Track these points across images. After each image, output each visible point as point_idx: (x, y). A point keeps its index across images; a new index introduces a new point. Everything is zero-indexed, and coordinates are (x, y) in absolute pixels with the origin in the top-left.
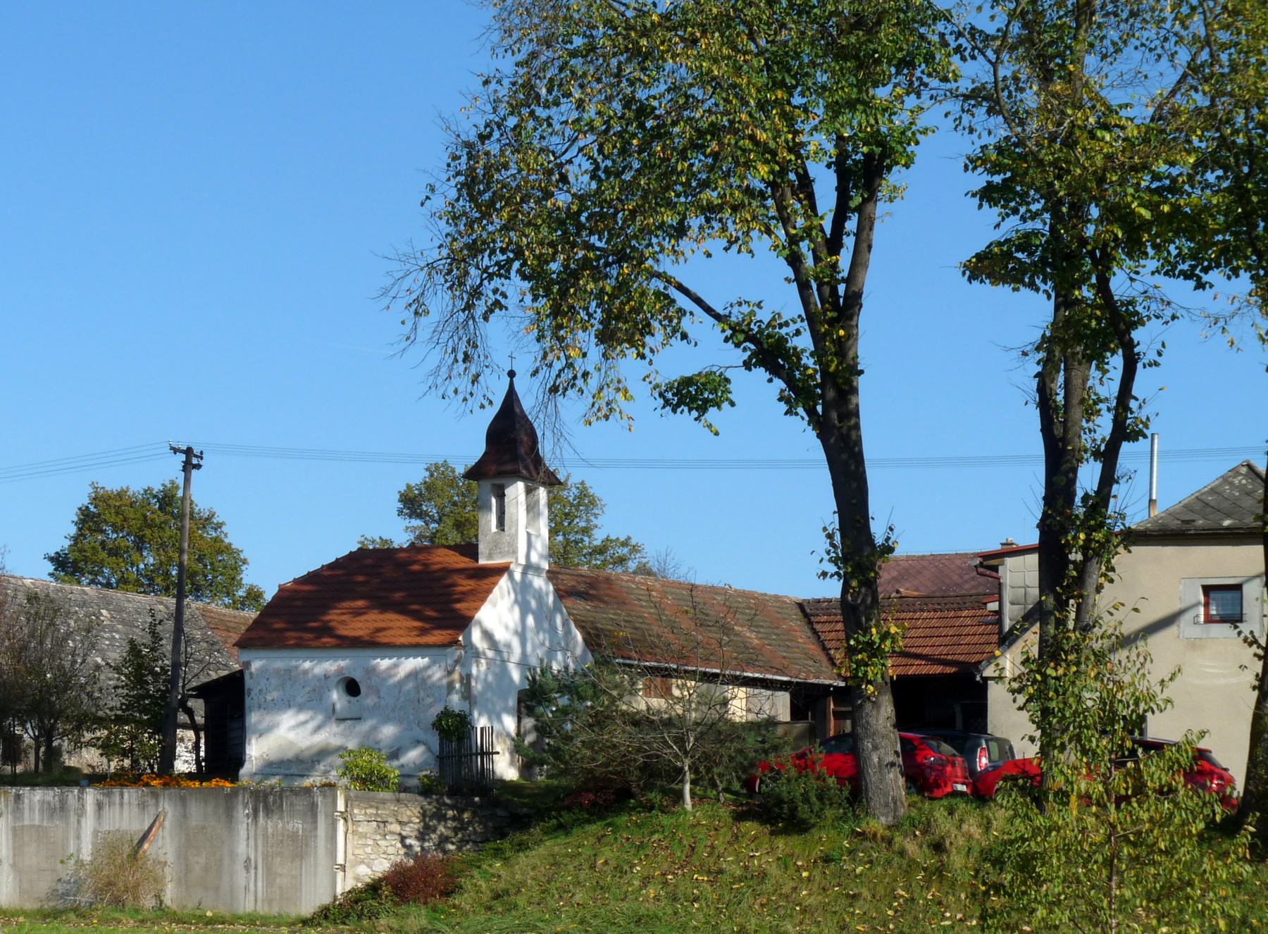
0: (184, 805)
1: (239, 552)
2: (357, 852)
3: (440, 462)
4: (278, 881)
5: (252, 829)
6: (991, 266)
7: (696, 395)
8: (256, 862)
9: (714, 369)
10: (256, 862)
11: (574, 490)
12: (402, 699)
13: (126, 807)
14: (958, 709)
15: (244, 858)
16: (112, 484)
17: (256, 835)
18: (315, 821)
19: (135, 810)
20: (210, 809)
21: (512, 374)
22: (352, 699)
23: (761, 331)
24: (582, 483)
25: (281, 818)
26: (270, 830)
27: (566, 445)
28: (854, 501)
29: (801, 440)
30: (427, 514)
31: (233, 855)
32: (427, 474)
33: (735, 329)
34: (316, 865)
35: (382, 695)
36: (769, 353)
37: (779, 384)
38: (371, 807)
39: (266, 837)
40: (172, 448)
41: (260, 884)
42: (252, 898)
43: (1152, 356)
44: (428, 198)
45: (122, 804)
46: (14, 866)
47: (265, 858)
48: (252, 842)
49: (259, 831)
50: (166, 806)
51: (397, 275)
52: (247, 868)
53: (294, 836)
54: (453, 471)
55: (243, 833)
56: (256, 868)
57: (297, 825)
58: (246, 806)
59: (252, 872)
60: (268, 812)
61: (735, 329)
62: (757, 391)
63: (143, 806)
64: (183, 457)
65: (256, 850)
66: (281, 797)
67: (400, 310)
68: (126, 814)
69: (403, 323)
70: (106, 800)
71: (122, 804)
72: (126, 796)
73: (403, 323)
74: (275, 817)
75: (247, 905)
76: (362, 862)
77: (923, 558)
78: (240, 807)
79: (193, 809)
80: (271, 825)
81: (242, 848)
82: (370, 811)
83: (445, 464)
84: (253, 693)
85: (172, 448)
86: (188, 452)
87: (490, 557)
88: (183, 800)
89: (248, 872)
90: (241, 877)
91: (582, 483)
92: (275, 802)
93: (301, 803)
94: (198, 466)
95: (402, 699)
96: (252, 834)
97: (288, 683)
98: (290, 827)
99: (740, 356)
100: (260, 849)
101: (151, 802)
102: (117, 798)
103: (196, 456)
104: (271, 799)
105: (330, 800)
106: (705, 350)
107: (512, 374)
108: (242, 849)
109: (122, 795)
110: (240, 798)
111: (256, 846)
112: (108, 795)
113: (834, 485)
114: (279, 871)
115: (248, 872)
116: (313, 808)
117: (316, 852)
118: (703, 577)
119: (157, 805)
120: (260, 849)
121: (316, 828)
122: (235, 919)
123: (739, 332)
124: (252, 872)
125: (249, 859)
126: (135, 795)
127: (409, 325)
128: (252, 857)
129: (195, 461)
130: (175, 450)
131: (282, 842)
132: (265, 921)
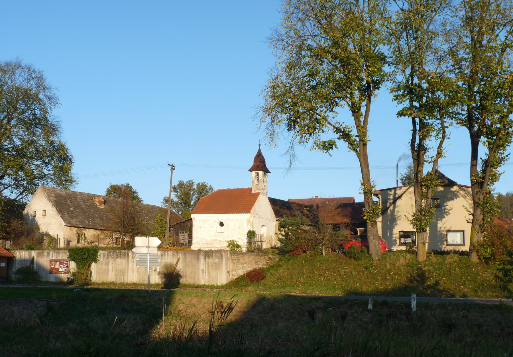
0: (185, 256)
6: (401, 114)
7: (328, 146)
14: (358, 230)
16: (115, 184)
19: (172, 256)
20: (193, 256)
21: (260, 145)
31: (199, 269)
36: (345, 136)
43: (448, 136)
46: (138, 272)
47: (208, 269)
53: (216, 264)
57: (217, 261)
58: (203, 255)
62: (342, 145)
63: (174, 255)
64: (171, 167)
67: (257, 121)
81: (201, 267)
88: (185, 254)
93: (218, 255)
99: (338, 136)
101: (176, 254)
102: (167, 253)
107: (260, 145)
112: (164, 253)
113: (228, 190)
116: (221, 256)
118: (324, 197)
123: (338, 130)
125: (203, 270)
130: (169, 165)
132: (208, 287)
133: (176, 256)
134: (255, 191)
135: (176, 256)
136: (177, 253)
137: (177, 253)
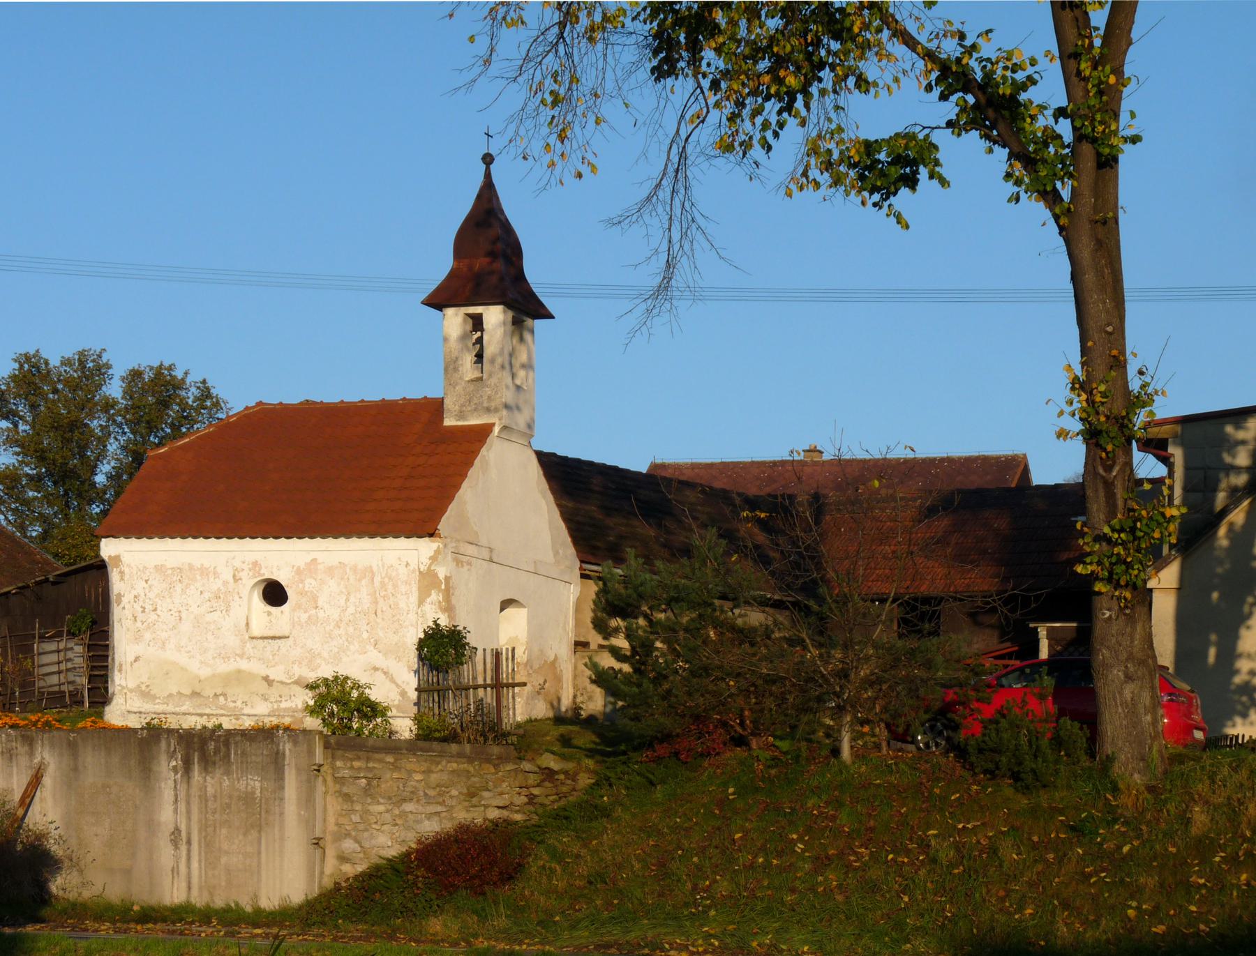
2: (342, 820)
3: (32, 352)
4: (224, 860)
5: (182, 789)
8: (189, 834)
10: (189, 834)
11: (193, 389)
12: (351, 610)
14: (1042, 633)
15: (171, 828)
17: (188, 796)
21: (488, 159)
22: (274, 609)
24: (204, 382)
25: (228, 773)
26: (210, 790)
27: (699, 236)
28: (1109, 329)
29: (1030, 241)
31: (152, 825)
32: (17, 366)
35: (320, 604)
36: (992, 107)
37: (1002, 153)
38: (359, 758)
39: (204, 798)
41: (195, 865)
42: (184, 885)
47: (203, 827)
48: (182, 807)
49: (194, 791)
50: (47, 755)
52: (175, 843)
54: (47, 363)
55: (167, 794)
56: (189, 842)
57: (254, 783)
58: (171, 756)
59: (184, 848)
60: (207, 763)
62: (974, 162)
65: (189, 819)
69: (472, 39)
73: (472, 39)
74: (218, 773)
75: (173, 894)
76: (348, 835)
77: (711, 466)
78: (163, 758)
79: (89, 759)
82: (356, 764)
84: (125, 600)
87: (461, 415)
88: (72, 747)
89: (176, 847)
90: (166, 854)
91: (204, 382)
92: (217, 751)
93: (259, 752)
95: (351, 610)
96: (182, 795)
97: (179, 587)
98: (242, 785)
100: (195, 816)
101: (22, 749)
104: (212, 746)
107: (488, 159)
108: (166, 815)
110: (163, 744)
111: (189, 812)
114: (225, 846)
115: (176, 847)
117: (282, 823)
119: (31, 754)
120: (195, 816)
121: (282, 788)
123: (951, 76)
125: (177, 830)
127: (483, 44)
128: (183, 827)
131: (229, 806)
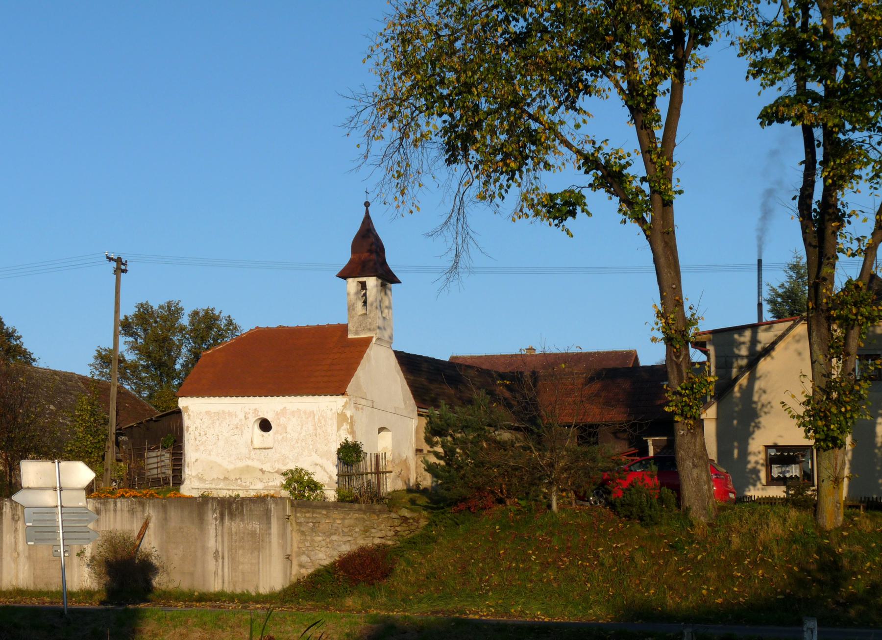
1: (30, 354)
2: (300, 545)
4: (241, 567)
5: (219, 529)
6: (770, 116)
8: (223, 554)
9: (575, 188)
10: (223, 554)
12: (304, 433)
13: (119, 513)
14: (650, 442)
18: (269, 523)
19: (126, 514)
21: (367, 204)
23: (608, 162)
25: (242, 520)
26: (234, 530)
27: (471, 242)
30: (136, 334)
31: (204, 549)
33: (586, 158)
34: (270, 555)
36: (611, 178)
37: (616, 199)
38: (308, 512)
39: (230, 534)
40: (108, 257)
41: (226, 570)
42: (220, 581)
44: (369, 56)
45: (115, 511)
47: (230, 550)
48: (219, 538)
49: (226, 530)
50: (151, 512)
51: (359, 109)
52: (216, 558)
53: (253, 534)
54: (152, 308)
55: (212, 532)
56: (223, 558)
58: (214, 511)
59: (220, 561)
61: (586, 158)
62: (603, 204)
63: (132, 512)
64: (114, 264)
65: (223, 545)
66: (242, 505)
67: (358, 135)
68: (119, 518)
69: (358, 146)
70: (102, 508)
71: (115, 511)
72: (119, 504)
73: (358, 146)
74: (238, 520)
75: (215, 586)
76: (304, 553)
77: (480, 357)
78: (210, 513)
79: (173, 514)
80: (234, 526)
83: (147, 303)
84: (190, 429)
85: (108, 257)
86: (119, 260)
87: (357, 333)
88: (164, 506)
89: (217, 560)
90: (211, 564)
92: (237, 508)
94: (125, 271)
95: (304, 433)
96: (219, 533)
98: (249, 527)
99: (590, 178)
100: (226, 544)
101: (139, 508)
102: (112, 506)
103: (123, 264)
104: (234, 506)
105: (281, 506)
106: (563, 175)
107: (367, 204)
109: (115, 503)
111: (223, 541)
114: (241, 560)
117: (270, 546)
119: (143, 511)
120: (226, 544)
121: (270, 528)
122: (203, 598)
123: (589, 162)
124: (220, 561)
125: (217, 551)
126: (126, 504)
127: (364, 148)
128: (220, 550)
129: (123, 267)
130: (110, 259)
131: (243, 538)
133: (139, 515)
134: (357, 333)
135: (139, 515)
136: (142, 504)
137: (142, 504)
